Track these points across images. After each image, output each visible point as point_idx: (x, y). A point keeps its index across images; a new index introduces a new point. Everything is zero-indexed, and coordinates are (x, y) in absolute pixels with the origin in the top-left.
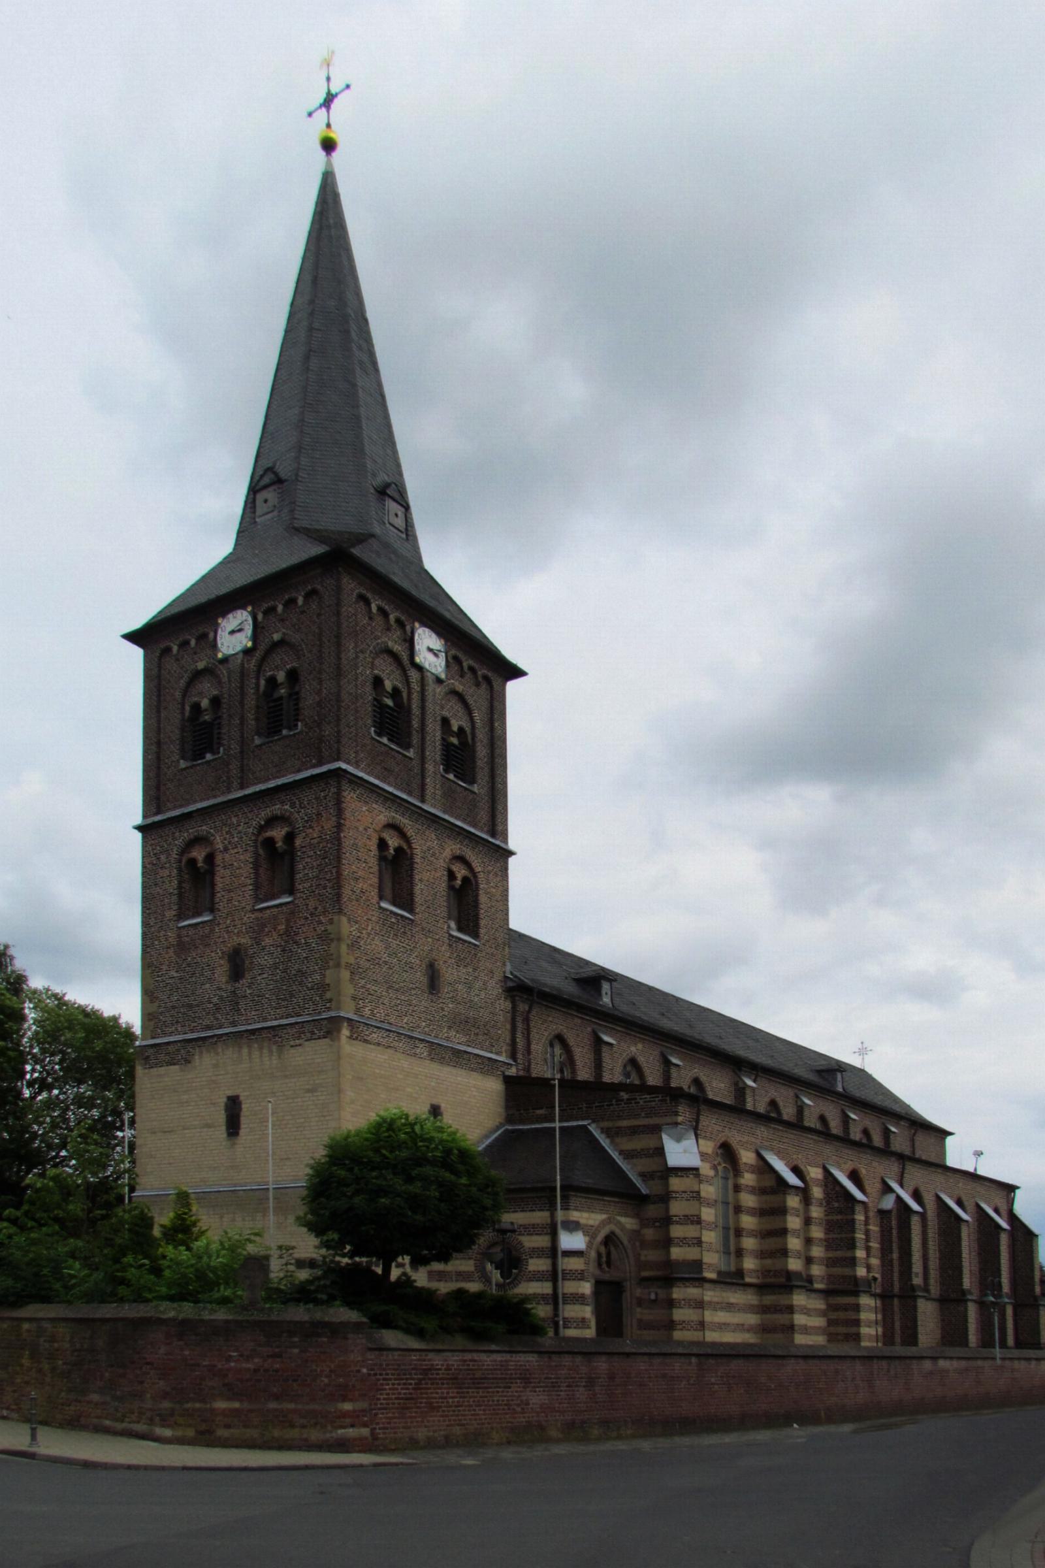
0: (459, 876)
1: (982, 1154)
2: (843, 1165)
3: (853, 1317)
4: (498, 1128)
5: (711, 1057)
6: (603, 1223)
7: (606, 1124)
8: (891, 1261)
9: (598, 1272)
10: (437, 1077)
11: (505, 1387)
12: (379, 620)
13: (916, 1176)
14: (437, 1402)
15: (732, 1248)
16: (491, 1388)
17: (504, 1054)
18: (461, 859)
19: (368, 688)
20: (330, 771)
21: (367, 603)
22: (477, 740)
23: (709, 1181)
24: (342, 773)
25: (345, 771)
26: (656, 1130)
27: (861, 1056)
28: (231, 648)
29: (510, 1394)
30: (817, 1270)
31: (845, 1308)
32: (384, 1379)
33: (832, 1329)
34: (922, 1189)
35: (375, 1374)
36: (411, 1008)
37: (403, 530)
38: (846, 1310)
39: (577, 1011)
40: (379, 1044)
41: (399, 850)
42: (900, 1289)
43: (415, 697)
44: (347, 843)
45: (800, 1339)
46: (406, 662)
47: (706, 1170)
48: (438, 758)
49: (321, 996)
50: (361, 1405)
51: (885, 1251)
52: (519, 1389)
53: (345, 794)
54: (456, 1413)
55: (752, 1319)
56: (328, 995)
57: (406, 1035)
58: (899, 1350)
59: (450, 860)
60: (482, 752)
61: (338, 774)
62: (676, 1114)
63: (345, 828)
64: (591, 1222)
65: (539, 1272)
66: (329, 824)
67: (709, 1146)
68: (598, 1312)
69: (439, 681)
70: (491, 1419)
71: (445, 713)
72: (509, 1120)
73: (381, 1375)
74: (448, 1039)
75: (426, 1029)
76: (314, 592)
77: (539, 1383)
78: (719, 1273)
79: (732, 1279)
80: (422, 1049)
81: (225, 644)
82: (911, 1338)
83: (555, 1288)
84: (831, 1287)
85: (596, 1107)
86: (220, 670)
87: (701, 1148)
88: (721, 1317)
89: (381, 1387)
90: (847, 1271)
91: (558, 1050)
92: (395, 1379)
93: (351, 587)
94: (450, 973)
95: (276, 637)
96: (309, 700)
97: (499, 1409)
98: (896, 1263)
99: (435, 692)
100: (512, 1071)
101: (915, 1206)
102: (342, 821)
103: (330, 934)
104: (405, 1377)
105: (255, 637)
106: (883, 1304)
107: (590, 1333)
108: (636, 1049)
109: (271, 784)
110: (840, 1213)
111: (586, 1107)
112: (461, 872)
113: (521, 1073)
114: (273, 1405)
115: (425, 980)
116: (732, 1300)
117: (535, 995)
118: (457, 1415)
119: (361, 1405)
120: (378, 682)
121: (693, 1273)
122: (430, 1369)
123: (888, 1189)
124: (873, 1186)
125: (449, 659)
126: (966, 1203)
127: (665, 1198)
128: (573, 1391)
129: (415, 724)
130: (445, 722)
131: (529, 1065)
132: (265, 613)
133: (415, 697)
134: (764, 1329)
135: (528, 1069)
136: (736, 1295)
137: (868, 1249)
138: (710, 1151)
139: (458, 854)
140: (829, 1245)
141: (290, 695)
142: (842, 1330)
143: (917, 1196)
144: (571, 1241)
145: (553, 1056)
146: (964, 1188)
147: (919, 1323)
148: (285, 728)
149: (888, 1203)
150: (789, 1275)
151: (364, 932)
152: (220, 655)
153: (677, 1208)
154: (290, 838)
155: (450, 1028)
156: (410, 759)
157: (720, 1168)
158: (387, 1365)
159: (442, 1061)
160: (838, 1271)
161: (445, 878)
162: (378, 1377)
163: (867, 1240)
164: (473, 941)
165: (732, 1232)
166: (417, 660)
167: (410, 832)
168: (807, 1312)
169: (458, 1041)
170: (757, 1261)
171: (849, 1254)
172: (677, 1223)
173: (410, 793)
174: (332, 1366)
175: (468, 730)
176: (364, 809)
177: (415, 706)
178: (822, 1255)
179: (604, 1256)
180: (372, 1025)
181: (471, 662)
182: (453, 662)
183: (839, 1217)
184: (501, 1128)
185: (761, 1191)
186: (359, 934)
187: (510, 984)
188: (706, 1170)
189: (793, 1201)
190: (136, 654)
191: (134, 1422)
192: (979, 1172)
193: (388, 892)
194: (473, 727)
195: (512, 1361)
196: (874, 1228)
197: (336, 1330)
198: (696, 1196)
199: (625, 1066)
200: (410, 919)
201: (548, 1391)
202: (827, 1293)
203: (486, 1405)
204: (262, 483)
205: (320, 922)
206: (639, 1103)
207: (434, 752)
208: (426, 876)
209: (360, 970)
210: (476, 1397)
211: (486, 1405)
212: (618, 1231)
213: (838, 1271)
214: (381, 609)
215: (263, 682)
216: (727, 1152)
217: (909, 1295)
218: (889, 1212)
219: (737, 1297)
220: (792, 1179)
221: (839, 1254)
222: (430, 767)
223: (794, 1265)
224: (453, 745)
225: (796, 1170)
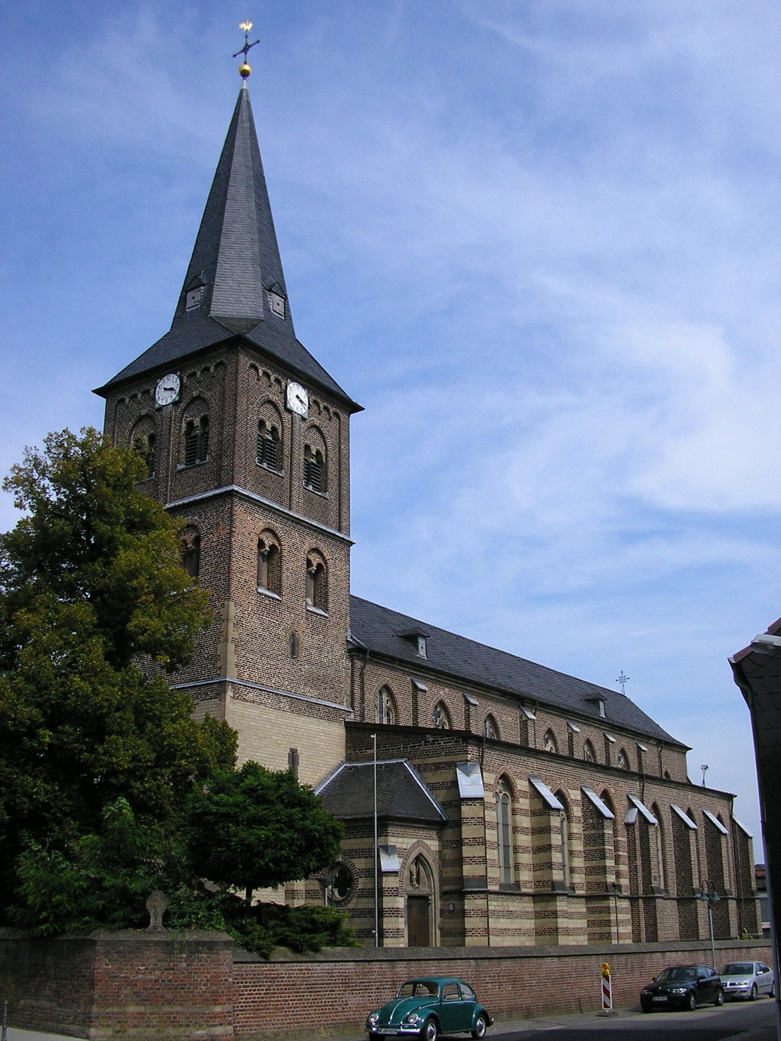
0: (315, 563)
1: (707, 768)
2: (596, 787)
3: (606, 919)
4: (340, 766)
5: (501, 696)
6: (414, 847)
7: (417, 761)
8: (636, 867)
9: (410, 888)
10: (295, 726)
11: (330, 991)
12: (265, 379)
13: (655, 792)
14: (281, 1005)
15: (512, 864)
16: (320, 992)
17: (345, 704)
18: (316, 550)
19: (255, 429)
20: (226, 492)
21: (257, 370)
22: (329, 459)
23: (493, 807)
24: (234, 493)
25: (237, 492)
26: (452, 765)
27: (622, 684)
28: (165, 400)
29: (334, 996)
30: (579, 879)
31: (600, 911)
32: (244, 987)
33: (592, 930)
34: (659, 803)
35: (238, 983)
36: (277, 671)
37: (282, 314)
38: (600, 912)
39: (399, 665)
40: (254, 702)
41: (273, 547)
42: (644, 891)
43: (287, 432)
44: (236, 545)
45: (563, 940)
46: (283, 409)
47: (489, 798)
48: (302, 475)
49: (214, 665)
50: (228, 1007)
51: (632, 858)
52: (341, 992)
53: (236, 508)
54: (295, 1013)
55: (530, 924)
56: (219, 664)
57: (273, 693)
58: (644, 945)
59: (309, 552)
60: (332, 468)
61: (232, 493)
62: (466, 753)
63: (235, 534)
64: (404, 846)
65: (366, 889)
66: (224, 532)
67: (491, 778)
68: (409, 923)
69: (303, 419)
70: (319, 1017)
71: (308, 442)
72: (349, 759)
73: (242, 983)
74: (304, 694)
75: (289, 687)
76: (221, 363)
77: (356, 986)
78: (501, 886)
79: (511, 891)
80: (284, 704)
81: (161, 398)
82: (653, 937)
83: (381, 902)
84: (590, 892)
85: (410, 747)
86: (156, 416)
87: (486, 781)
88: (503, 923)
89: (242, 993)
90: (599, 878)
91: (385, 697)
92: (252, 986)
93: (245, 361)
94: (306, 640)
95: (195, 394)
96: (213, 440)
97: (326, 1009)
98: (640, 869)
99: (301, 427)
100: (351, 718)
101: (652, 818)
102: (233, 529)
103: (222, 615)
104: (258, 984)
105: (180, 393)
106: (632, 905)
107: (403, 943)
108: (444, 693)
109: (186, 501)
110: (594, 828)
111: (403, 748)
112: (316, 560)
113: (358, 719)
114: (167, 1009)
115: (289, 647)
116: (511, 909)
117: (368, 654)
118: (296, 1015)
119: (228, 1007)
120: (262, 424)
121: (481, 887)
122: (276, 978)
123: (632, 805)
124: (620, 803)
125: (311, 404)
126: (695, 813)
127: (458, 824)
128: (381, 992)
129: (286, 452)
130: (307, 447)
131: (363, 713)
132: (188, 377)
133: (287, 432)
134: (539, 932)
135: (362, 715)
136: (515, 904)
137: (617, 860)
138: (492, 782)
139: (314, 547)
140: (588, 856)
141: (202, 435)
142: (597, 929)
143: (655, 809)
144: (389, 863)
145: (381, 703)
146: (691, 798)
147: (658, 921)
148: (198, 458)
149: (632, 817)
150: (554, 885)
151: (246, 612)
152: (157, 406)
153: (467, 832)
154: (197, 541)
155: (306, 685)
156: (282, 478)
157: (501, 795)
158: (247, 975)
159: (299, 712)
160: (593, 878)
161: (305, 566)
162: (240, 984)
163: (616, 849)
164: (323, 613)
165: (511, 849)
166: (288, 406)
167: (280, 533)
168: (569, 916)
169: (311, 694)
170: (531, 873)
171: (602, 864)
172: (468, 844)
173: (281, 504)
174: (209, 976)
175: (323, 453)
176: (249, 518)
177: (287, 442)
178: (582, 865)
179: (415, 873)
180: (249, 687)
181: (326, 404)
182: (313, 404)
183: (594, 832)
184: (342, 765)
185: (534, 813)
186: (242, 615)
187: (351, 647)
188: (489, 798)
189: (555, 821)
190: (103, 401)
191: (71, 1023)
192: (706, 787)
193: (264, 581)
194: (326, 450)
195: (336, 969)
196: (622, 839)
197: (211, 946)
198: (482, 821)
199: (436, 707)
200: (278, 600)
201: (362, 993)
202: (588, 898)
203: (316, 1006)
204: (192, 286)
205: (215, 606)
206: (440, 743)
207: (299, 471)
208: (291, 565)
209: (242, 643)
210: (309, 999)
211: (316, 1006)
212: (425, 853)
213: (593, 878)
214: (265, 373)
215: (184, 425)
216: (506, 780)
217: (650, 897)
218: (633, 824)
219: (515, 905)
220: (555, 802)
221: (594, 863)
222: (295, 483)
223: (557, 875)
224: (312, 463)
225: (560, 795)
